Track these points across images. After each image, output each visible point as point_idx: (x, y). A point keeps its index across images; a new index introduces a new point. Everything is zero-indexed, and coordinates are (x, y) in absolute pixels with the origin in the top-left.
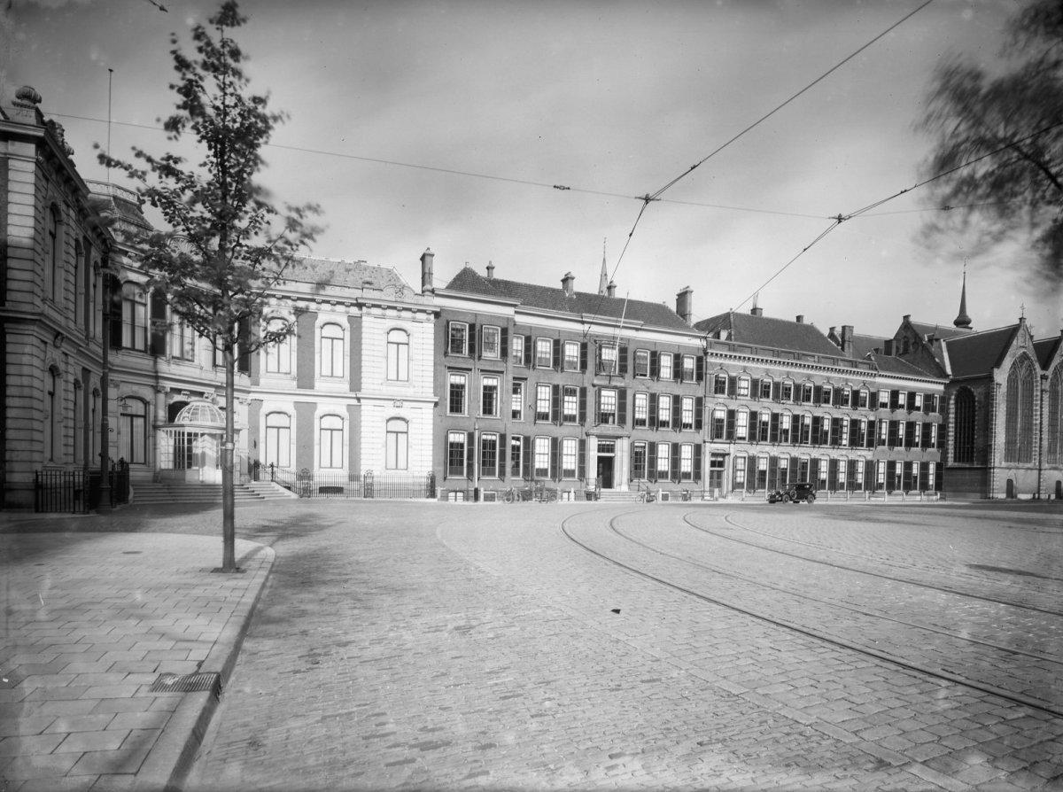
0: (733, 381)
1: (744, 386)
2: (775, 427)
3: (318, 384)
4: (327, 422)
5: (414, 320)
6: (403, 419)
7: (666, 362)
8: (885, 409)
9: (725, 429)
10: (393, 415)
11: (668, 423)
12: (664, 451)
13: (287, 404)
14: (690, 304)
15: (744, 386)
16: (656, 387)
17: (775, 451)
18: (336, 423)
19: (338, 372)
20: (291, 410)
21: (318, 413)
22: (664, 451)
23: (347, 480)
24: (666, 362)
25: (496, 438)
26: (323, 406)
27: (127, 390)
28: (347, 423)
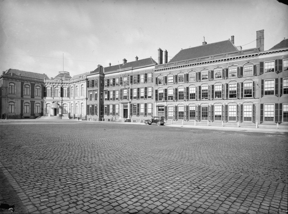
0: (166, 78)
1: (171, 79)
2: (166, 94)
3: (35, 97)
4: (26, 104)
5: (16, 81)
6: (13, 102)
7: (142, 77)
8: (273, 72)
9: (165, 96)
10: (26, 102)
11: (143, 97)
12: (142, 106)
13: (29, 101)
14: (159, 54)
15: (171, 79)
16: (139, 86)
17: (187, 103)
18: (38, 105)
19: (28, 94)
20: (30, 102)
21: (35, 103)
22: (142, 106)
23: (30, 115)
24: (142, 77)
25: (208, 107)
26: (36, 101)
27: (47, 103)
28: (41, 105)
